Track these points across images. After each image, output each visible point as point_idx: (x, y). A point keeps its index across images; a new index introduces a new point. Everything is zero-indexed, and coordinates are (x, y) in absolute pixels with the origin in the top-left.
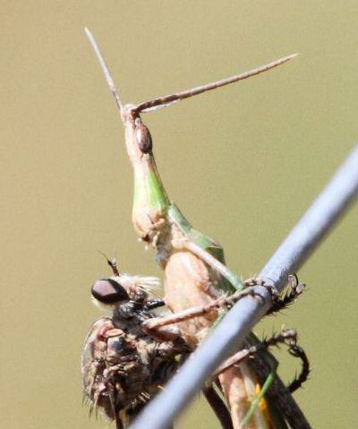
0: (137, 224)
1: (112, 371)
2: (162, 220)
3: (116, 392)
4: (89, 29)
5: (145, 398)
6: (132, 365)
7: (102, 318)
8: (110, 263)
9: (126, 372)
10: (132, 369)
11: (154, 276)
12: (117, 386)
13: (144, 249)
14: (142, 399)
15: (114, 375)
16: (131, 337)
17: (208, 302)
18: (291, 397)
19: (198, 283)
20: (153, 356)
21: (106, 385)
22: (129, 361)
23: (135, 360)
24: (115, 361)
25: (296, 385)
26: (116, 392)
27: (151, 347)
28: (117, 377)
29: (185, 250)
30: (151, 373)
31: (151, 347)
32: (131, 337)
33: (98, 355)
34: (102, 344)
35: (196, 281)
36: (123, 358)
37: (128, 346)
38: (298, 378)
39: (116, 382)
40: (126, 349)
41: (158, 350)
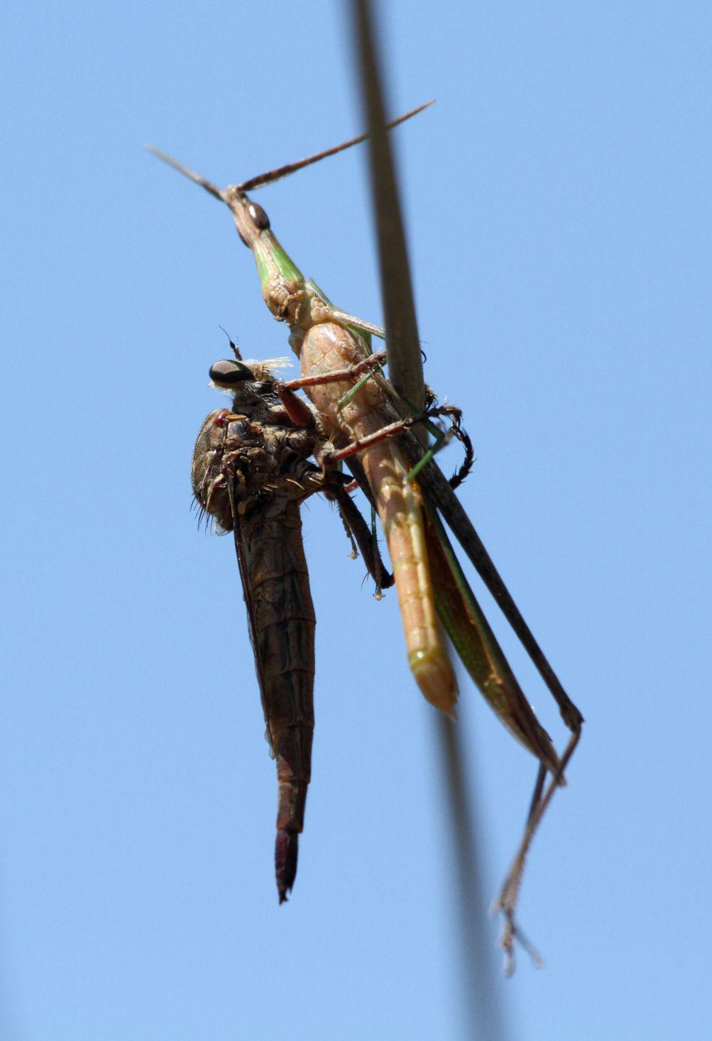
0: (195, 459)
1: (232, 455)
2: (299, 476)
3: (236, 480)
4: (440, 509)
5: (270, 488)
6: (257, 450)
7: (224, 398)
8: (232, 345)
9: (250, 457)
10: (257, 455)
11: (287, 356)
12: (238, 472)
13: (241, 470)
14: (267, 489)
15: (235, 461)
16: (256, 424)
17: (395, 530)
18: (453, 496)
19: (343, 350)
20: (281, 444)
21: (225, 472)
22: (253, 446)
23: (260, 446)
24: (234, 446)
25: (456, 481)
26: (236, 480)
27: (280, 434)
28: (239, 463)
29: (327, 320)
30: (279, 463)
31: (280, 434)
32: (256, 424)
33: (215, 442)
34: (221, 430)
35: (340, 348)
36: (245, 442)
37: (253, 431)
38: (457, 474)
39: (236, 468)
40: (251, 436)
41: (288, 439)
